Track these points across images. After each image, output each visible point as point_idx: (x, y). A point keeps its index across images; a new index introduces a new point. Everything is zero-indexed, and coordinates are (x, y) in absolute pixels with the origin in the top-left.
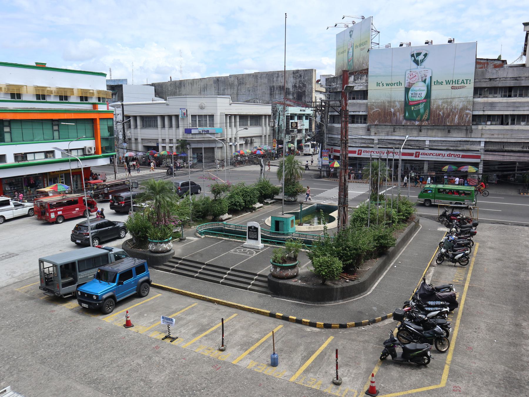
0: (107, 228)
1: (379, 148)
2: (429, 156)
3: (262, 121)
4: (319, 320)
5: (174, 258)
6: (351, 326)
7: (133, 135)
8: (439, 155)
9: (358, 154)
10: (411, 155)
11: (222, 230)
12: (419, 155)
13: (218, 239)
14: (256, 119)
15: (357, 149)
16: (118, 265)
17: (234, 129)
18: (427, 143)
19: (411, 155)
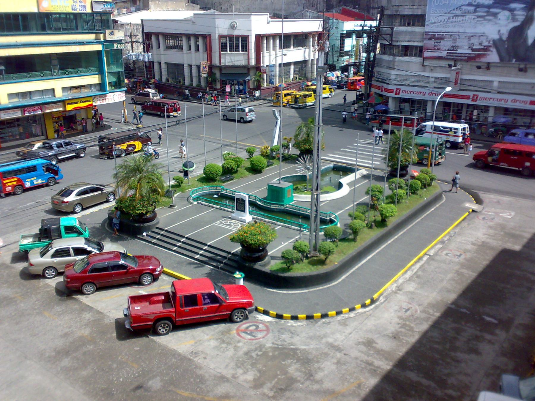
0: (205, 316)
1: (435, 87)
2: (488, 102)
3: (309, 42)
4: (273, 309)
5: (157, 228)
6: (303, 319)
7: (155, 57)
8: (420, 93)
9: (473, 100)
10: (467, 97)
11: (223, 197)
12: (399, 92)
13: (210, 206)
14: (300, 39)
15: (471, 94)
16: (16, 102)
17: (273, 53)
18: (496, 84)
19: (467, 97)
